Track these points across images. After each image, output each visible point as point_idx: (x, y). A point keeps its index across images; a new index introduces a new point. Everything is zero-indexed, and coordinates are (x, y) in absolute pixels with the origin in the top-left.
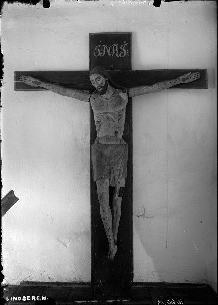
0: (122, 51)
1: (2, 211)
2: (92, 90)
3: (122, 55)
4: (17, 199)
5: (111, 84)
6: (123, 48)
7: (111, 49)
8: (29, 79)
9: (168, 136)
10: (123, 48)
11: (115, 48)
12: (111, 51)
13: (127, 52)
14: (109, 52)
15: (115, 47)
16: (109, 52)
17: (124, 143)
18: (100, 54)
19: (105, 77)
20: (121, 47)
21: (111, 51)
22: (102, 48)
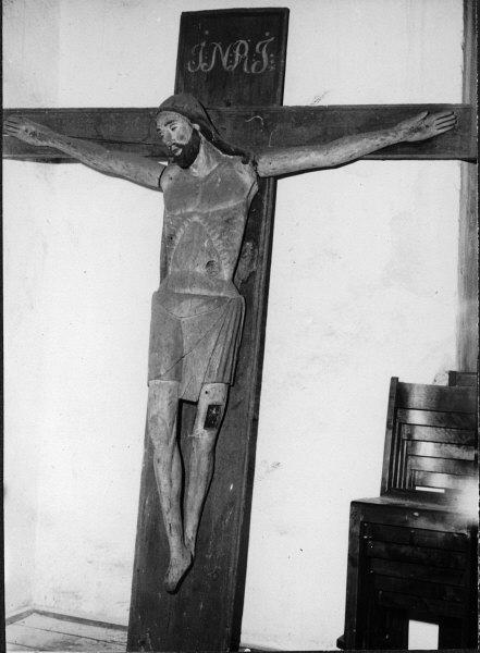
0: (259, 57)
1: (476, 379)
2: (158, 151)
3: (259, 68)
4: (353, 503)
5: (209, 137)
6: (261, 47)
7: (231, 52)
8: (24, 128)
9: (180, 381)
10: (261, 47)
11: (242, 52)
12: (231, 58)
13: (269, 59)
14: (225, 60)
15: (243, 47)
16: (225, 60)
17: (231, 294)
18: (202, 65)
19: (192, 119)
20: (258, 46)
21: (231, 58)
22: (208, 51)
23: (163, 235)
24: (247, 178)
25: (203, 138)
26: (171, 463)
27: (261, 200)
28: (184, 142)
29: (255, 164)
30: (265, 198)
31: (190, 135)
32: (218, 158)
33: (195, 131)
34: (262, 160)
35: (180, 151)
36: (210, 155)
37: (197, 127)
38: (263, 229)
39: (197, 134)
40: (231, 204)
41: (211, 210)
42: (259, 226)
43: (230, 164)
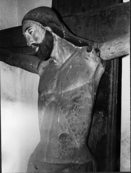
19: (44, 24)
23: (40, 128)
24: (92, 63)
25: (57, 37)
26: (29, 54)
27: (108, 77)
28: (40, 41)
29: (97, 51)
30: (111, 76)
31: (43, 36)
32: (71, 49)
33: (47, 33)
34: (103, 47)
35: (37, 49)
36: (64, 48)
37: (49, 29)
38: (110, 100)
39: (51, 35)
40: (79, 84)
41: (63, 92)
42: (108, 98)
43: (80, 53)
